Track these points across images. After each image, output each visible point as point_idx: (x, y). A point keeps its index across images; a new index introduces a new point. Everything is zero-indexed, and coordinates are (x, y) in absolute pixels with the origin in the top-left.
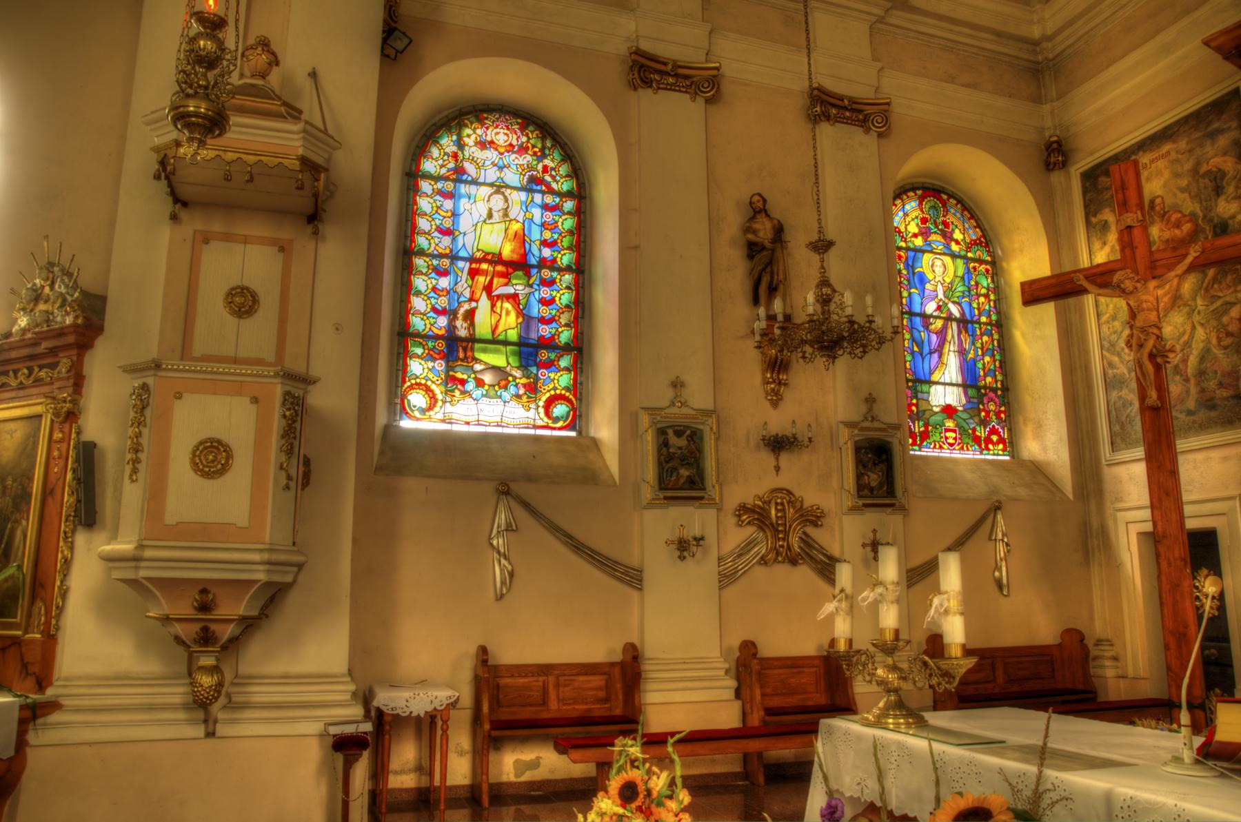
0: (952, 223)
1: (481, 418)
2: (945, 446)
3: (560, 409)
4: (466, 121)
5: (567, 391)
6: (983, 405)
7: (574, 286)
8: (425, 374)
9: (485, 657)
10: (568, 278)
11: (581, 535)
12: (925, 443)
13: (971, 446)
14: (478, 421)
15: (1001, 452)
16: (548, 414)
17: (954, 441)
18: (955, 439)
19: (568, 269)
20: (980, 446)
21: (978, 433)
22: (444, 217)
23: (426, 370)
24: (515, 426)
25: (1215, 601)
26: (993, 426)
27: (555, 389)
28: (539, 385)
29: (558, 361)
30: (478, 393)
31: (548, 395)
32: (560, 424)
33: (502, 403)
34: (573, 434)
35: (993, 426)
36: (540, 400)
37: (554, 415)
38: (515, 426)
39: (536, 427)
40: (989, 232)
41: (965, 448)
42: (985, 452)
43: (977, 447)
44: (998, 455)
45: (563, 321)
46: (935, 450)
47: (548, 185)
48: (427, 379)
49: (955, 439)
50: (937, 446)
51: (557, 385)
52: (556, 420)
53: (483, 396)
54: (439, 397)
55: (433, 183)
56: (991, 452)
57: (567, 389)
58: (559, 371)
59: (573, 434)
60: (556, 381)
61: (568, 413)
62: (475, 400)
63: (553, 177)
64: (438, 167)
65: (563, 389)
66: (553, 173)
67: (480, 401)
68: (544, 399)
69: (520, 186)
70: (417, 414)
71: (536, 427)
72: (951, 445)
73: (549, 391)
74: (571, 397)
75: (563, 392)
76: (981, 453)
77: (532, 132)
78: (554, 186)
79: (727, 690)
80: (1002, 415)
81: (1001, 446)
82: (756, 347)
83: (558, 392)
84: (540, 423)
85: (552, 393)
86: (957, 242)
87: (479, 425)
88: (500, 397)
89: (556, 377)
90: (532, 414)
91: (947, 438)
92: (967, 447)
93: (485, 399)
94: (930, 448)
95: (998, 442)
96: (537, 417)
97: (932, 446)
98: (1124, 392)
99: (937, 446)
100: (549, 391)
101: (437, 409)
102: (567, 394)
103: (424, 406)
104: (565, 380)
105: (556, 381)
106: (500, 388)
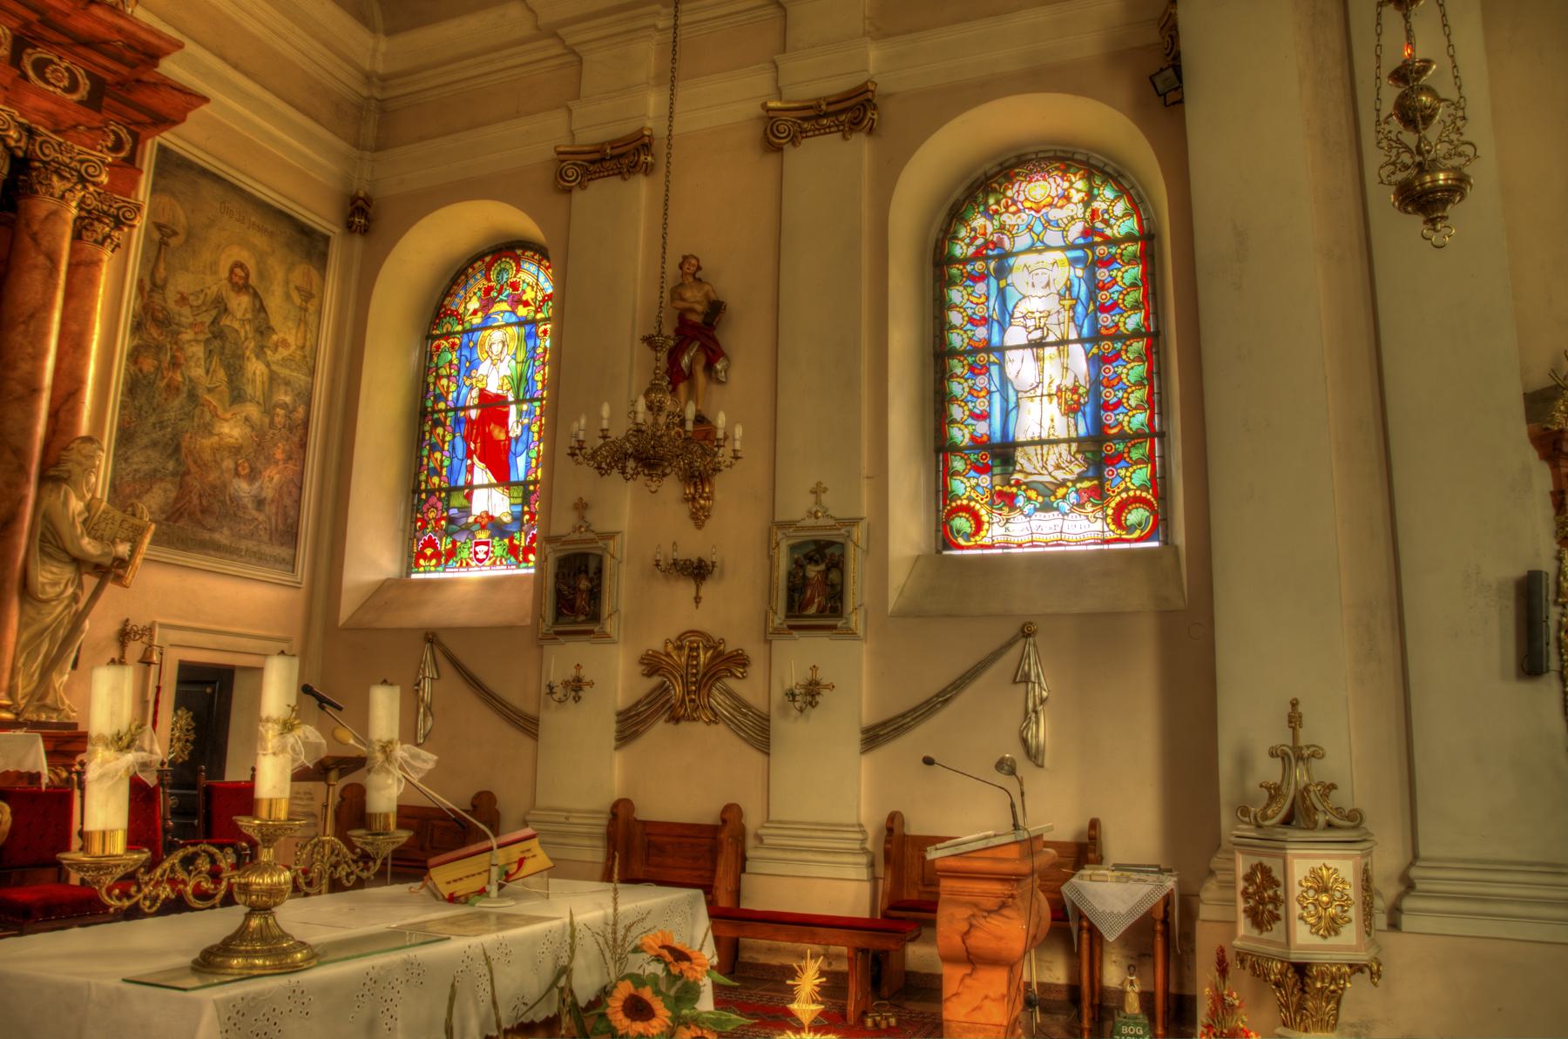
0: (524, 282)
1: (1036, 537)
2: (473, 563)
3: (1136, 515)
4: (995, 185)
5: (1142, 491)
6: (529, 507)
7: (1146, 355)
8: (967, 494)
9: (1093, 832)
10: (1138, 346)
11: (492, 684)
12: (451, 562)
13: (506, 560)
14: (1032, 541)
15: (432, 569)
16: (1118, 521)
17: (484, 556)
18: (487, 553)
19: (1136, 334)
20: (516, 557)
21: (516, 542)
22: (977, 304)
23: (969, 489)
24: (1077, 543)
25: (188, 744)
26: (430, 537)
27: (1127, 490)
28: (1107, 487)
29: (1129, 452)
30: (1028, 509)
31: (1118, 499)
32: (1137, 534)
33: (1061, 516)
34: (1155, 544)
35: (430, 537)
36: (1108, 506)
37: (1128, 523)
38: (1077, 543)
39: (1108, 542)
40: (440, 290)
41: (498, 563)
42: (523, 565)
43: (513, 559)
44: (430, 572)
45: (1133, 402)
46: (461, 569)
47: (1101, 234)
48: (970, 499)
49: (487, 553)
50: (464, 564)
51: (1129, 484)
52: (1130, 529)
53: (1036, 510)
54: (985, 518)
55: (961, 267)
56: (422, 569)
57: (1142, 487)
58: (1132, 465)
59: (1155, 544)
60: (1128, 479)
61: (1147, 519)
62: (1026, 516)
63: (1106, 222)
64: (965, 247)
65: (1138, 488)
66: (1106, 216)
67: (1033, 517)
68: (1113, 504)
69: (1063, 244)
70: (961, 541)
71: (1108, 542)
72: (481, 561)
73: (1119, 494)
74: (1149, 497)
75: (1138, 493)
76: (518, 567)
77: (1075, 175)
78: (1108, 232)
79: (753, 871)
80: (443, 523)
81: (434, 562)
82: (569, 454)
83: (1131, 493)
84: (1113, 536)
85: (1124, 495)
86: (526, 304)
87: (1033, 546)
88: (1057, 509)
89: (1128, 474)
90: (1098, 525)
91: (476, 553)
92: (501, 561)
93: (1038, 514)
94: (455, 567)
95: (432, 556)
96: (1106, 529)
97: (458, 565)
98: (968, 436)
99: (464, 564)
100: (1119, 494)
101: (983, 533)
102: (1144, 494)
103: (969, 530)
104: (1141, 475)
105: (1128, 479)
106: (1056, 498)
